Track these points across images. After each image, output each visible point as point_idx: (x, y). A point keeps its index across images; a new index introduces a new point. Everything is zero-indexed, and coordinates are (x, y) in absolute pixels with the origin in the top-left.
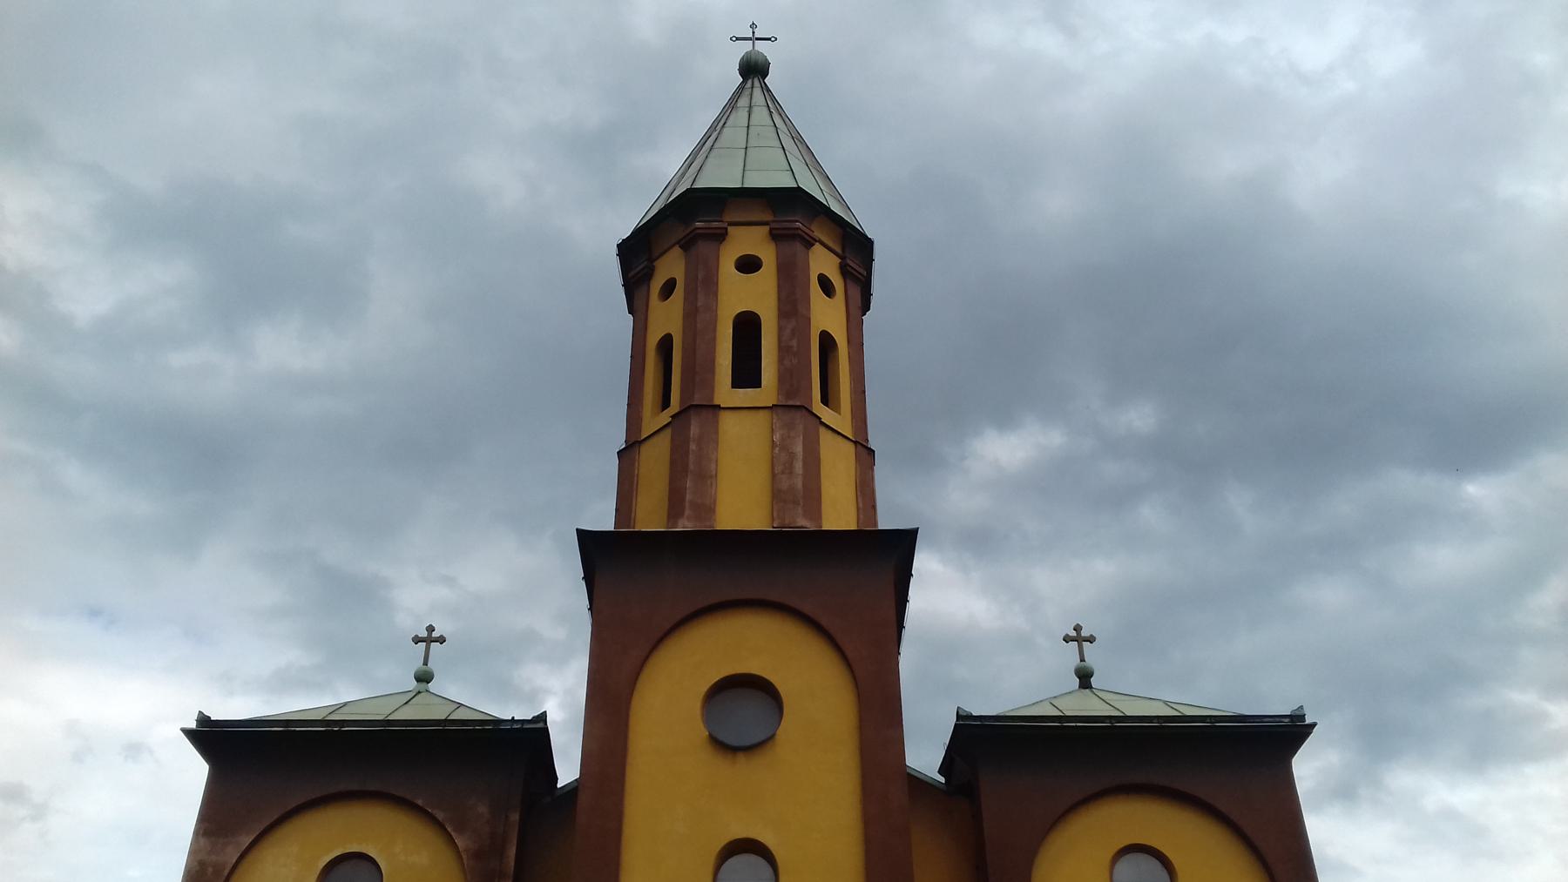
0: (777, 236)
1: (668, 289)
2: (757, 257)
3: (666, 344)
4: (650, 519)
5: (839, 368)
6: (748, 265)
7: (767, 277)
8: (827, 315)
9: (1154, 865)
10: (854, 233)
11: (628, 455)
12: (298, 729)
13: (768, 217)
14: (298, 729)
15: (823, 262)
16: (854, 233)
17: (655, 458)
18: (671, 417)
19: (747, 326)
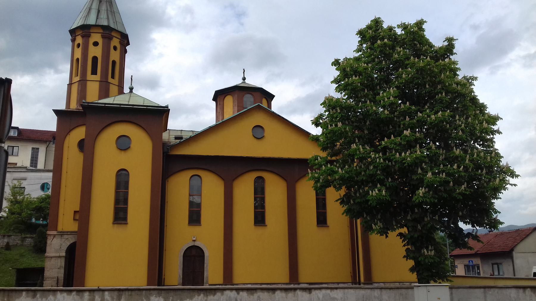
0: (103, 37)
1: (79, 45)
2: (96, 41)
3: (78, 59)
4: (74, 106)
5: (364, 278)
6: (96, 44)
7: (100, 48)
8: (115, 56)
9: (197, 177)
10: (165, 158)
11: (70, 85)
12: (98, 105)
13: (102, 31)
14: (98, 105)
15: (115, 42)
16: (165, 158)
17: (75, 88)
18: (170, 109)
19: (95, 59)
